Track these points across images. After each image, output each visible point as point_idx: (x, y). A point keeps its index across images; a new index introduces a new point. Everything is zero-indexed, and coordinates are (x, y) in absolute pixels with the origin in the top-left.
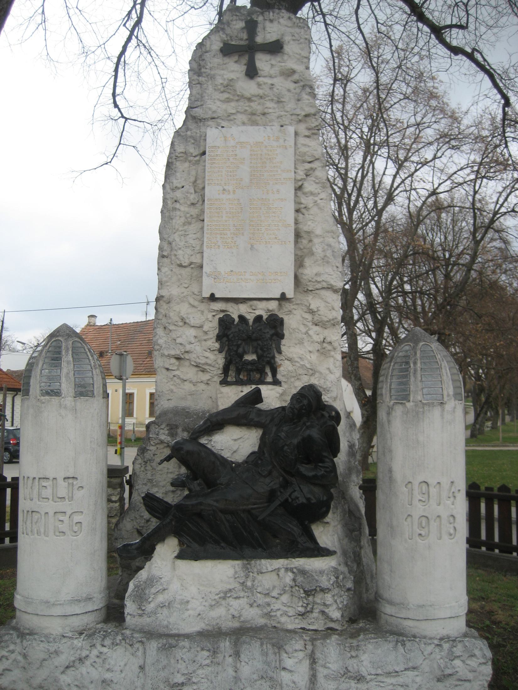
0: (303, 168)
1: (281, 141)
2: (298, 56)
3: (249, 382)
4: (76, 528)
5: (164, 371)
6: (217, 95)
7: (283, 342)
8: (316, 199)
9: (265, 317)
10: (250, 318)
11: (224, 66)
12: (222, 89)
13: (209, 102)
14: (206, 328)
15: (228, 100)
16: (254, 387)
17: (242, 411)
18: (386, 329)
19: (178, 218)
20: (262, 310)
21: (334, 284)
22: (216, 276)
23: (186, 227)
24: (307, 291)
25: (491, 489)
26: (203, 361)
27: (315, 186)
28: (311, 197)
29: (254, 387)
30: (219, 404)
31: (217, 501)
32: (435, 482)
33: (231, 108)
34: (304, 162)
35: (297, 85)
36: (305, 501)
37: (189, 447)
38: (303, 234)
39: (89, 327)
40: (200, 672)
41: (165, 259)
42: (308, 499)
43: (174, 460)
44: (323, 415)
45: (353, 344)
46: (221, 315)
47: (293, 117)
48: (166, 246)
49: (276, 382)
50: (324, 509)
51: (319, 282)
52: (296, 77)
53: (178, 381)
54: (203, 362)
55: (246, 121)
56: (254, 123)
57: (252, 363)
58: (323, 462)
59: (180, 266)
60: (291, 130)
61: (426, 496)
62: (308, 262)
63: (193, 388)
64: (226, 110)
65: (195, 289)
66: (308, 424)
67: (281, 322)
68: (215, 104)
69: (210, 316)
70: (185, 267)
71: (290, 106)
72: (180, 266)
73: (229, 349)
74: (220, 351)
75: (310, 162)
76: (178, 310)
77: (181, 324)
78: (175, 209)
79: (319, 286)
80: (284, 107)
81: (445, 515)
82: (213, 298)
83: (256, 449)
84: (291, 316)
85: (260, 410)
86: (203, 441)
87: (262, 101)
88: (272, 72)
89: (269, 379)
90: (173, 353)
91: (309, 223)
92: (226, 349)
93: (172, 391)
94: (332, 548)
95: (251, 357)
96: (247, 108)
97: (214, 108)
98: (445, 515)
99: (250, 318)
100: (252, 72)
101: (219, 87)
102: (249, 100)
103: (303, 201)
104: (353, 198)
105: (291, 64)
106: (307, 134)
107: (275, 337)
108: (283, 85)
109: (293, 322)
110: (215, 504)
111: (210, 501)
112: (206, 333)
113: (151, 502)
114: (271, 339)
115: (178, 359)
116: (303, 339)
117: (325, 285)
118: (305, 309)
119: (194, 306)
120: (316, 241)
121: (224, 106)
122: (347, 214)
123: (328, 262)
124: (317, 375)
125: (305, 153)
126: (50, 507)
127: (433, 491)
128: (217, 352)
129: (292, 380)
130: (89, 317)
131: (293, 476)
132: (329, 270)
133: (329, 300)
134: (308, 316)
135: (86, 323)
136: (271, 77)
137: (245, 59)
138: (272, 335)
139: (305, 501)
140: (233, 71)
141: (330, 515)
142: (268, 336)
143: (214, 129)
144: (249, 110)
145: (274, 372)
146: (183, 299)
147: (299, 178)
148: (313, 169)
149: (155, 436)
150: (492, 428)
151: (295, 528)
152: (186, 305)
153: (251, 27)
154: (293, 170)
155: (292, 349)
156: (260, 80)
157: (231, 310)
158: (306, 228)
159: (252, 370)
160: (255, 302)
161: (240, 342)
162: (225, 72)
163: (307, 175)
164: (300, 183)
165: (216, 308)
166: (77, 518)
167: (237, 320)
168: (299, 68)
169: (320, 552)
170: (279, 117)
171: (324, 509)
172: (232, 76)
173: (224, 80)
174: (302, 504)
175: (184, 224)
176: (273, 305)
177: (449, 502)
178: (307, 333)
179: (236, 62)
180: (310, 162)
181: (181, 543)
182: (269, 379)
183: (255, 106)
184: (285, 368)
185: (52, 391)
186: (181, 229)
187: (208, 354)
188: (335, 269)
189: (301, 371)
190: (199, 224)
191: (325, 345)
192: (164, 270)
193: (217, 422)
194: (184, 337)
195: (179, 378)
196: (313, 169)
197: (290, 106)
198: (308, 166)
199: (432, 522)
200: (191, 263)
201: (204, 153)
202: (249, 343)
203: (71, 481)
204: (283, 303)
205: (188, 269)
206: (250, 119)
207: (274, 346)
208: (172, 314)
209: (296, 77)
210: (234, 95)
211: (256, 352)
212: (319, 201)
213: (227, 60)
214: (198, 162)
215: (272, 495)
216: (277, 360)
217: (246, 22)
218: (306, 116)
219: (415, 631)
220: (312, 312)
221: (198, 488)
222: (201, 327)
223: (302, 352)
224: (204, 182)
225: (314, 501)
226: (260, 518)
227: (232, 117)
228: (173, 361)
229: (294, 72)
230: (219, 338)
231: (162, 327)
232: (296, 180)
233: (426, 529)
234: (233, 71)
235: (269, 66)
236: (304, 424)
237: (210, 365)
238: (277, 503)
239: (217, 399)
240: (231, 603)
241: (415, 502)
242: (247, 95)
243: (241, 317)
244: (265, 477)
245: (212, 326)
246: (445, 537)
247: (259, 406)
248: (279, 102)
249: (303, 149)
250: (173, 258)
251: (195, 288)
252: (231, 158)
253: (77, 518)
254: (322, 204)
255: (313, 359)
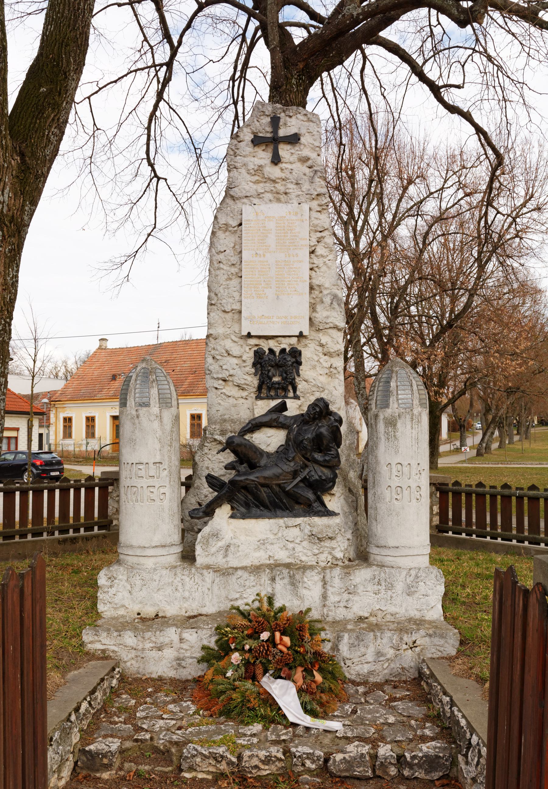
0: (315, 237)
1: (299, 215)
2: (312, 146)
3: (277, 397)
4: (162, 497)
5: (214, 390)
6: (249, 178)
7: (301, 367)
8: (325, 260)
9: (288, 350)
10: (277, 350)
11: (254, 154)
12: (253, 173)
13: (243, 183)
14: (244, 358)
15: (257, 182)
16: (280, 401)
17: (274, 416)
18: (392, 350)
19: (222, 275)
20: (285, 344)
21: (338, 324)
22: (251, 319)
23: (228, 282)
24: (319, 330)
25: (470, 486)
26: (243, 382)
27: (324, 250)
28: (321, 259)
29: (280, 401)
30: (255, 413)
31: (257, 477)
32: (406, 463)
33: (260, 188)
34: (316, 231)
35: (311, 170)
36: (317, 477)
37: (237, 440)
38: (315, 287)
39: (100, 351)
40: (248, 590)
41: (213, 306)
42: (320, 477)
43: (228, 451)
44: (330, 419)
45: (360, 365)
46: (256, 348)
47: (307, 196)
48: (213, 295)
49: (296, 397)
50: (331, 484)
51: (327, 323)
52: (309, 163)
53: (224, 397)
54: (242, 383)
55: (272, 199)
56: (279, 200)
57: (278, 383)
58: (331, 451)
59: (224, 311)
60: (306, 207)
61: (401, 473)
62: (319, 308)
63: (235, 402)
64: (256, 191)
65: (236, 328)
66: (320, 424)
67: (300, 353)
68: (246, 184)
69: (247, 349)
70: (228, 312)
71: (306, 186)
72: (224, 311)
73: (262, 373)
74: (255, 374)
75: (321, 232)
76: (223, 344)
77: (226, 355)
78: (219, 269)
79: (328, 326)
80: (301, 188)
81: (414, 486)
82: (249, 336)
83: (283, 443)
84: (307, 348)
85: (286, 416)
86: (247, 437)
87: (284, 182)
88: (292, 159)
89: (291, 394)
90: (220, 376)
91: (320, 278)
92: (260, 373)
93: (220, 404)
94: (336, 511)
95: (276, 379)
96: (273, 189)
97: (247, 187)
98: (414, 486)
99: (277, 350)
100: (276, 160)
101: (251, 171)
102: (274, 181)
103: (315, 262)
104: (360, 223)
105: (306, 152)
106: (319, 209)
107: (295, 365)
108: (300, 169)
109: (308, 353)
110: (256, 479)
111: (252, 477)
112: (244, 361)
113: (212, 480)
114: (292, 365)
115: (225, 380)
116: (315, 365)
117: (332, 325)
118: (317, 343)
119: (235, 342)
120: (325, 292)
121: (255, 187)
122: (356, 203)
123: (334, 308)
124: (326, 391)
125: (317, 225)
126: (144, 483)
127: (406, 469)
128: (253, 376)
129: (308, 395)
130: (100, 340)
131: (309, 461)
132: (334, 314)
133: (334, 336)
134: (320, 349)
135: (97, 346)
136: (291, 163)
137: (270, 149)
138: (293, 363)
139: (317, 477)
140: (261, 158)
141: (335, 488)
142: (290, 363)
143: (248, 206)
144: (275, 190)
145: (295, 389)
146: (226, 337)
147: (312, 244)
148: (323, 237)
149: (210, 436)
150: (500, 447)
151: (311, 495)
152: (230, 341)
153: (275, 122)
154: (308, 238)
155: (308, 373)
156: (283, 165)
157: (262, 344)
158: (317, 283)
159: (278, 388)
160: (280, 339)
161: (269, 368)
162: (256, 159)
163: (318, 242)
164: (313, 248)
165: (252, 343)
166: (162, 490)
167: (267, 351)
168: (313, 155)
169: (330, 514)
170: (298, 196)
171: (331, 484)
172: (262, 162)
173: (255, 165)
174: (316, 480)
175: (226, 280)
176: (294, 341)
177: (417, 477)
178: (318, 361)
179: (263, 150)
180: (321, 232)
181: (233, 508)
182: (291, 394)
183: (280, 187)
184: (301, 386)
185: (144, 403)
186: (224, 283)
187: (246, 377)
188: (339, 313)
189: (314, 389)
190: (239, 280)
191: (332, 369)
192: (212, 314)
193: (255, 425)
194: (228, 364)
195: (225, 394)
196: (323, 237)
197: (306, 186)
198: (319, 235)
199: (404, 490)
200: (232, 310)
201: (241, 224)
202: (276, 369)
203: (158, 465)
204: (301, 339)
205: (230, 314)
206: (275, 197)
207: (294, 370)
208: (219, 348)
209: (309, 163)
210: (262, 178)
211: (281, 375)
212: (328, 262)
213: (256, 149)
214: (235, 232)
215: (295, 474)
216: (296, 381)
217: (271, 118)
218: (318, 195)
219: (393, 564)
220: (322, 345)
221: (244, 470)
222: (241, 357)
223: (315, 375)
224: (241, 247)
225: (324, 478)
226: (287, 489)
227: (261, 196)
228: (221, 382)
229: (308, 159)
230: (254, 365)
231: (211, 357)
232: (311, 246)
233: (401, 495)
234: (261, 158)
235: (290, 154)
236: (317, 425)
237: (248, 385)
238: (299, 479)
239: (253, 409)
240: (268, 547)
241: (393, 477)
242: (273, 177)
243: (271, 351)
244: (290, 461)
245: (249, 357)
246: (414, 501)
247: (285, 413)
248: (297, 184)
249: (316, 222)
250: (219, 305)
251: (236, 328)
252: (261, 229)
253: (162, 490)
254: (330, 264)
255: (321, 379)
